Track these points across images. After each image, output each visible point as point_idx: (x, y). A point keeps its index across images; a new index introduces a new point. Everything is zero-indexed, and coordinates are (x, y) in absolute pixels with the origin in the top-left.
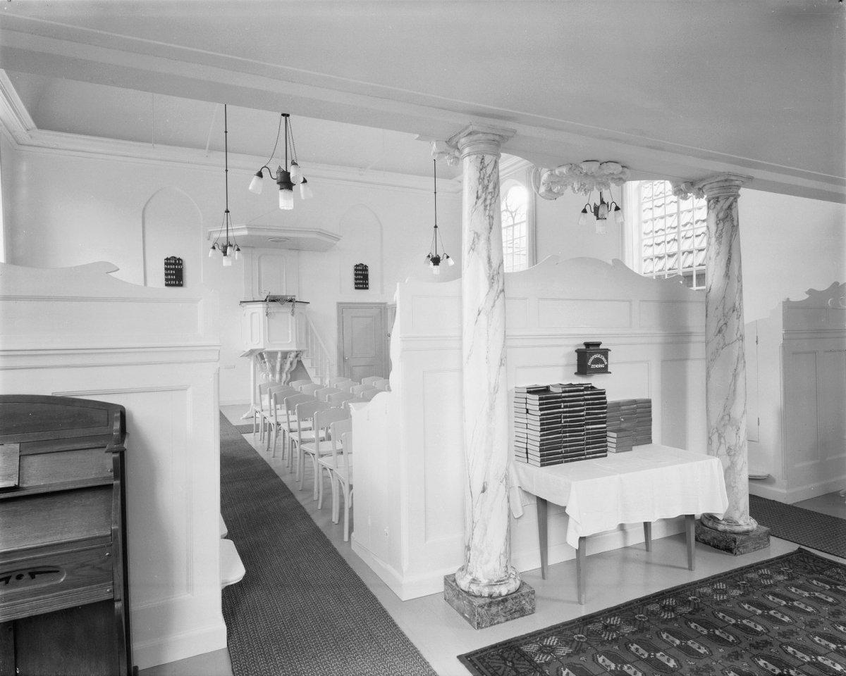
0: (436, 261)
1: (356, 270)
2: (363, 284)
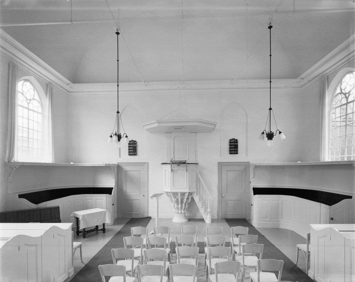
0: (270, 136)
1: (230, 142)
2: (234, 151)
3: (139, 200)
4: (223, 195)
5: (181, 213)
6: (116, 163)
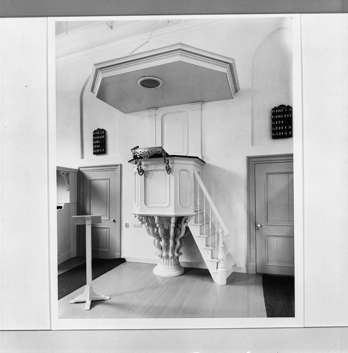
2: (283, 130)
3: (107, 228)
4: (259, 226)
5: (167, 257)
6: (77, 168)
